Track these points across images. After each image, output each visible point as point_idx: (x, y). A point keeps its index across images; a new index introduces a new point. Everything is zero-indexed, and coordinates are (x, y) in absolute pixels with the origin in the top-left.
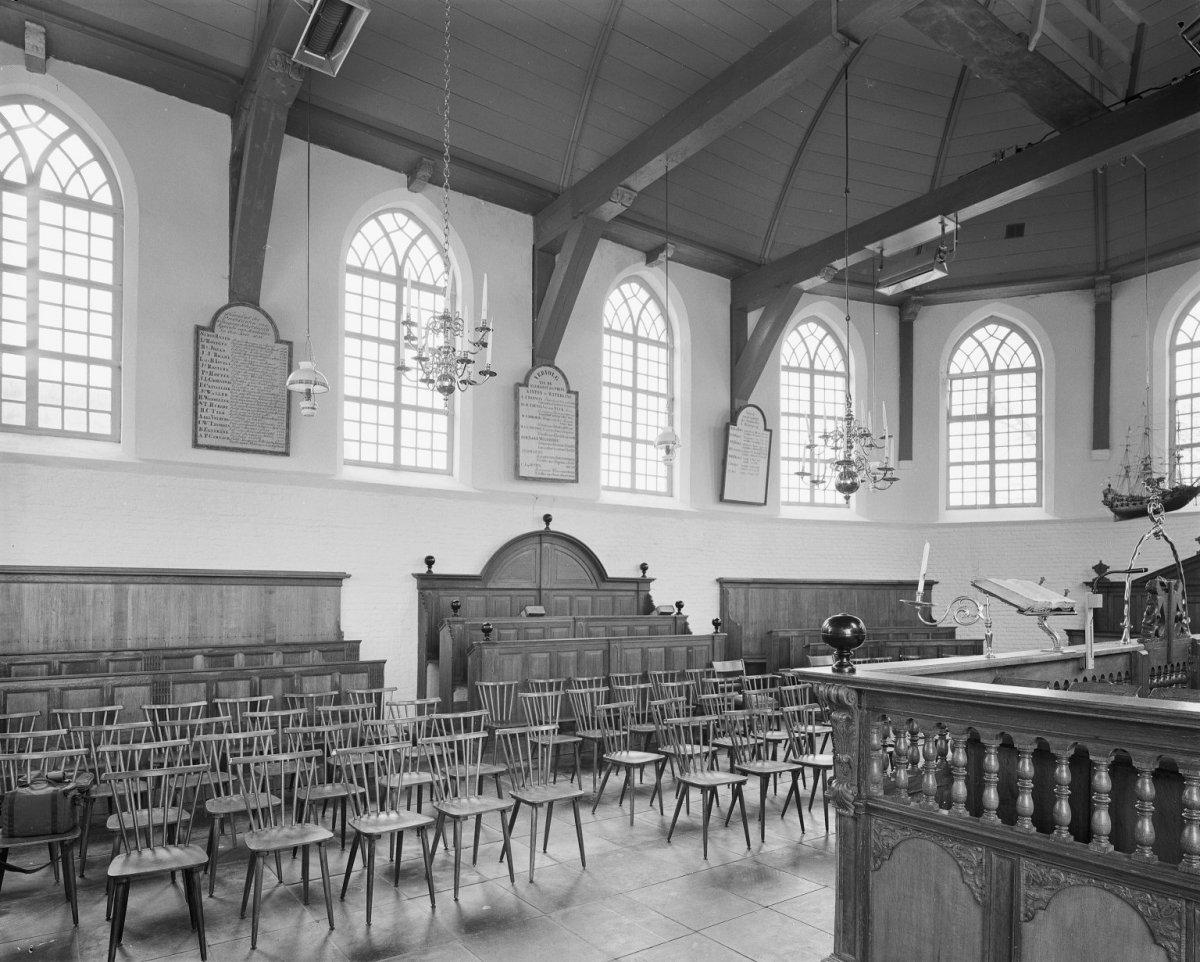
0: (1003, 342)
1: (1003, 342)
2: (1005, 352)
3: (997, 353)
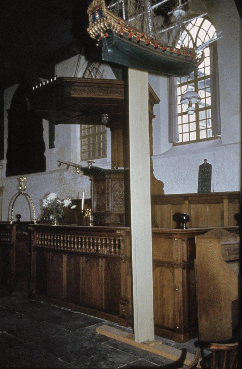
0: (200, 27)
1: (200, 27)
2: (202, 34)
3: (197, 36)
